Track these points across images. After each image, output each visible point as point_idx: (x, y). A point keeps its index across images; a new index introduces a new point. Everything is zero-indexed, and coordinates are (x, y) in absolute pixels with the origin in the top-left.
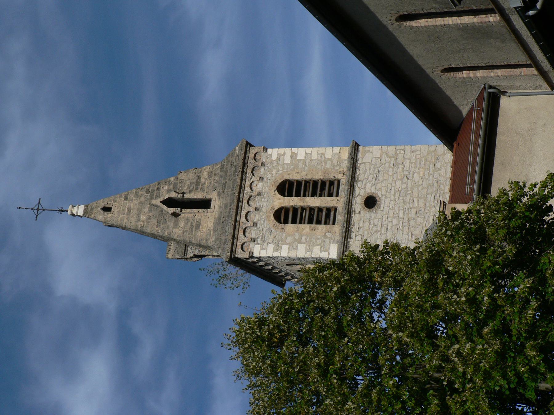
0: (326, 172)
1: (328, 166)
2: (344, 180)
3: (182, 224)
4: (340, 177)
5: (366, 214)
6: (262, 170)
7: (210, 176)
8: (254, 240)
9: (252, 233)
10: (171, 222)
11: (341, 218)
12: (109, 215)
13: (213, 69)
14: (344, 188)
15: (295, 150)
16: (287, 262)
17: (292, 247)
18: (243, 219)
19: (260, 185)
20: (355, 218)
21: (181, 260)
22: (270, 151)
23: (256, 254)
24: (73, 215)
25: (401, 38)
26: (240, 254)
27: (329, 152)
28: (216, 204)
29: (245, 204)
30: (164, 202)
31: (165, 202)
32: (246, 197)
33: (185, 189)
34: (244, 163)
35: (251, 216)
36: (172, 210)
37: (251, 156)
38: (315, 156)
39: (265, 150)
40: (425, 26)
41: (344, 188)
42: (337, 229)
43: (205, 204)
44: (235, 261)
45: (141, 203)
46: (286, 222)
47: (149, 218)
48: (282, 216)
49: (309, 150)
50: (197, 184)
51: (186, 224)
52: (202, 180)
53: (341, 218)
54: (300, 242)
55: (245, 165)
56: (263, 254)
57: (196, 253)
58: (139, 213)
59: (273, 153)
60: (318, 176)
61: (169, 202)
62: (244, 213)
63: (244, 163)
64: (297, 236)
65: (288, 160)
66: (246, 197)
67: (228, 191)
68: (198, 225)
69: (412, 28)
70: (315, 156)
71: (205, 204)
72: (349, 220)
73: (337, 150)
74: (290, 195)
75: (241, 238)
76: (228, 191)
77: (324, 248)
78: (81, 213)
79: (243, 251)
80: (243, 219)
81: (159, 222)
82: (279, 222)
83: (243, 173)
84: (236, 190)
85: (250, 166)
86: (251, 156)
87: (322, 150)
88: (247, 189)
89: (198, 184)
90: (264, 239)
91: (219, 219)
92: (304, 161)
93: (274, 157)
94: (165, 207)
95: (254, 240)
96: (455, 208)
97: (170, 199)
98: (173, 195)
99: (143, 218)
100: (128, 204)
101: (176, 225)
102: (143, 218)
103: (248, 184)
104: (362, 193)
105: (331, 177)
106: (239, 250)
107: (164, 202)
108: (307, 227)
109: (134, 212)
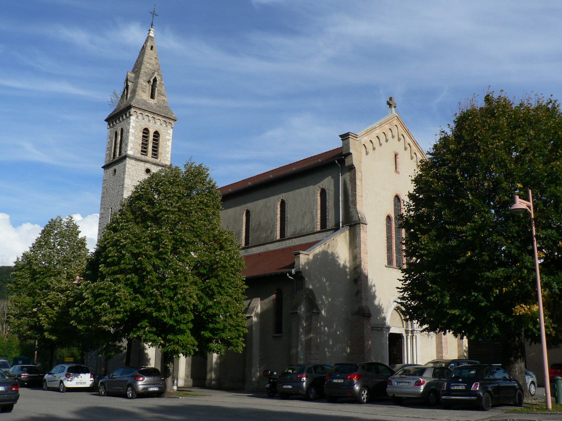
0: (161, 153)
1: (164, 155)
2: (157, 161)
4: (159, 159)
5: (144, 169)
6: (164, 125)
8: (137, 117)
9: (140, 117)
10: (146, 79)
11: (143, 157)
12: (149, 48)
13: (79, 37)
14: (154, 160)
15: (171, 141)
16: (125, 130)
17: (133, 134)
18: (146, 114)
19: (159, 124)
20: (142, 164)
21: (125, 78)
22: (172, 130)
23: (132, 117)
24: (150, 30)
25: (238, 208)
26: (132, 110)
27: (169, 156)
28: (152, 101)
29: (152, 116)
30: (155, 78)
32: (155, 116)
35: (147, 118)
36: (152, 80)
37: (171, 122)
38: (168, 149)
39: (172, 128)
41: (154, 160)
42: (139, 155)
43: (152, 97)
44: (130, 107)
45: (153, 65)
46: (143, 133)
47: (147, 68)
48: (146, 131)
49: (170, 147)
50: (160, 94)
52: (162, 97)
53: (143, 157)
54: (135, 138)
55: (168, 118)
56: (132, 121)
57: (130, 87)
58: (150, 64)
59: (171, 131)
60: (160, 150)
61: (155, 80)
62: (149, 114)
64: (137, 137)
65: (167, 137)
66: (155, 116)
67: (158, 109)
68: (144, 92)
69: (243, 214)
70: (168, 149)
71: (152, 97)
72: (142, 161)
73: (169, 159)
74: (154, 136)
75: (139, 112)
76: (158, 109)
77: (132, 148)
78: (151, 34)
80: (146, 114)
82: (144, 130)
85: (167, 120)
86: (171, 122)
87: (170, 153)
88: (158, 118)
89: (160, 94)
90: (137, 122)
92: (166, 144)
93: (169, 131)
94: (153, 78)
95: (137, 117)
98: (158, 83)
99: (148, 65)
101: (144, 81)
102: (148, 65)
103: (160, 118)
104: (152, 168)
105: (159, 156)
106: (135, 110)
107: (155, 78)
108: (140, 142)
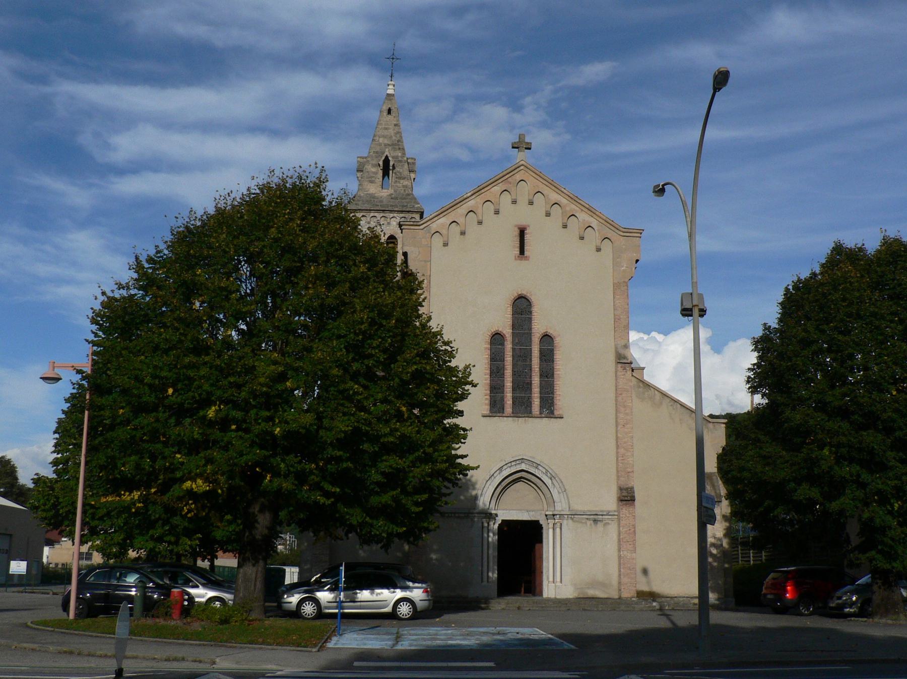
3: (374, 170)
7: (404, 186)
18: (372, 214)
29: (382, 215)
30: (387, 157)
31: (387, 158)
33: (397, 169)
34: (408, 212)
36: (381, 163)
40: (531, 384)
51: (374, 173)
52: (402, 181)
58: (384, 137)
62: (376, 214)
63: (408, 212)
68: (372, 182)
79: (478, 467)
80: (372, 214)
81: (377, 152)
83: (402, 212)
84: (390, 208)
88: (392, 215)
91: (374, 197)
96: (372, 593)
97: (389, 161)
98: (391, 163)
99: (381, 140)
100: (392, 127)
101: (374, 166)
102: (381, 140)
103: (395, 215)
109: (386, 133)
